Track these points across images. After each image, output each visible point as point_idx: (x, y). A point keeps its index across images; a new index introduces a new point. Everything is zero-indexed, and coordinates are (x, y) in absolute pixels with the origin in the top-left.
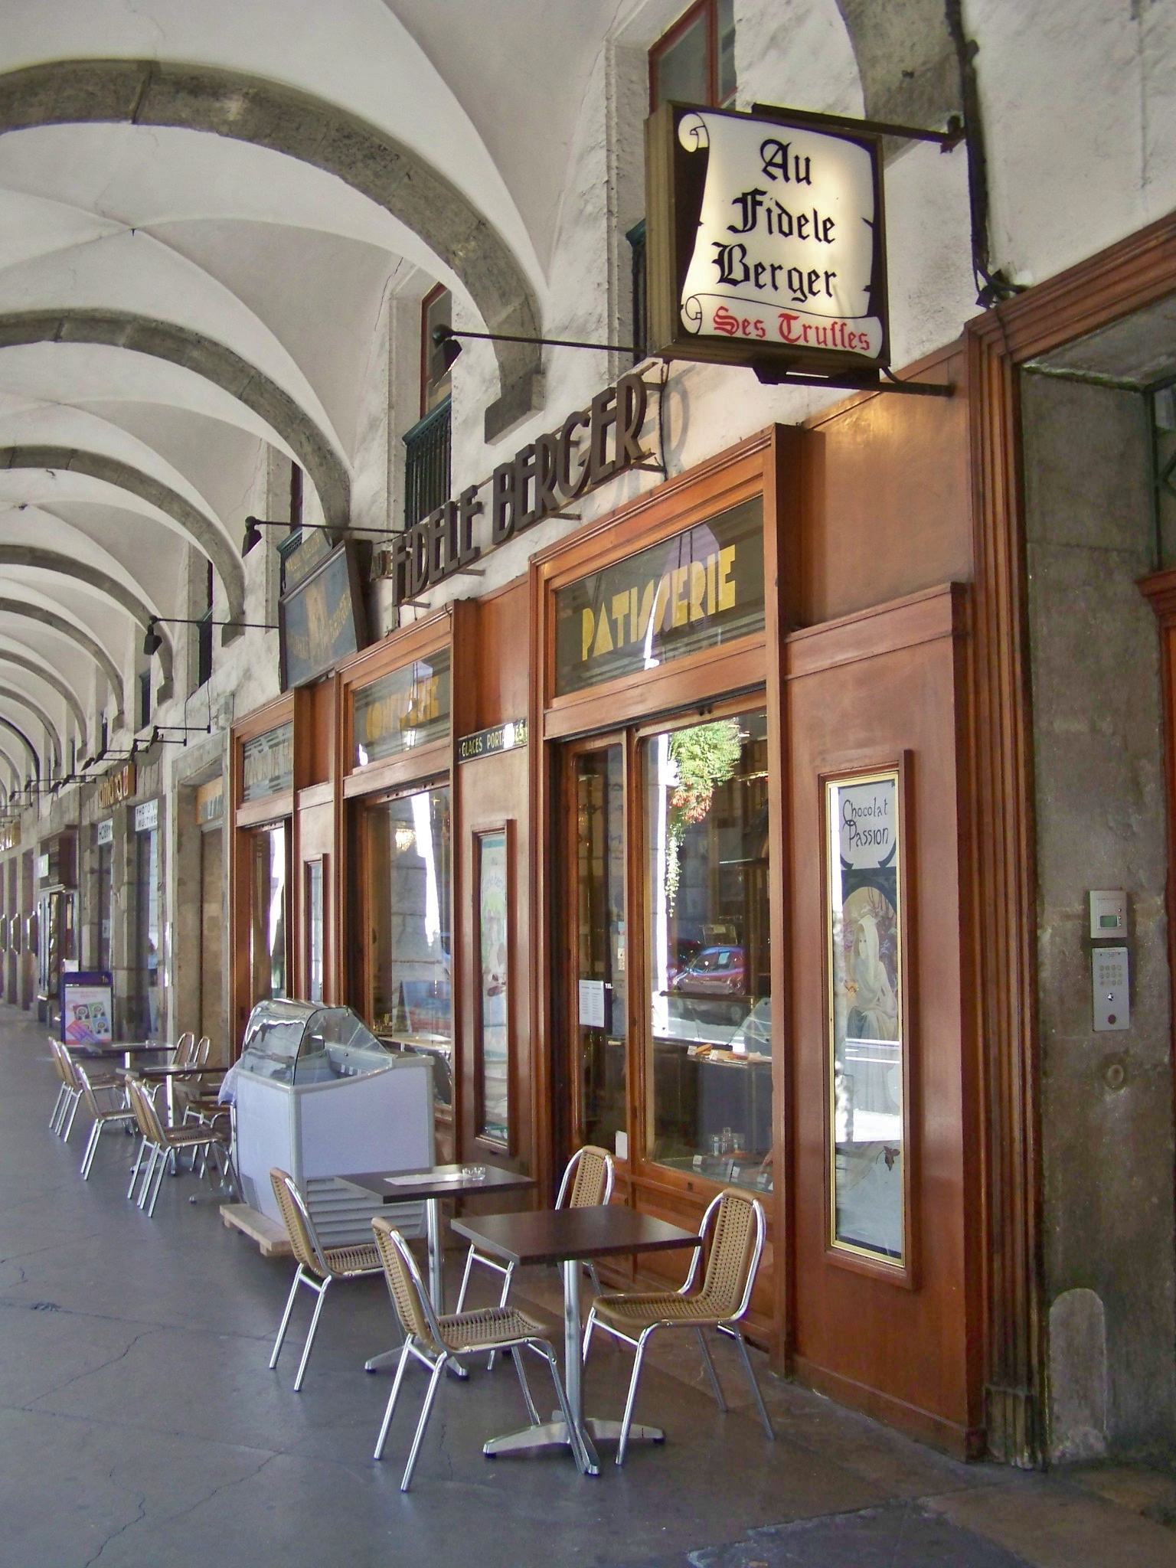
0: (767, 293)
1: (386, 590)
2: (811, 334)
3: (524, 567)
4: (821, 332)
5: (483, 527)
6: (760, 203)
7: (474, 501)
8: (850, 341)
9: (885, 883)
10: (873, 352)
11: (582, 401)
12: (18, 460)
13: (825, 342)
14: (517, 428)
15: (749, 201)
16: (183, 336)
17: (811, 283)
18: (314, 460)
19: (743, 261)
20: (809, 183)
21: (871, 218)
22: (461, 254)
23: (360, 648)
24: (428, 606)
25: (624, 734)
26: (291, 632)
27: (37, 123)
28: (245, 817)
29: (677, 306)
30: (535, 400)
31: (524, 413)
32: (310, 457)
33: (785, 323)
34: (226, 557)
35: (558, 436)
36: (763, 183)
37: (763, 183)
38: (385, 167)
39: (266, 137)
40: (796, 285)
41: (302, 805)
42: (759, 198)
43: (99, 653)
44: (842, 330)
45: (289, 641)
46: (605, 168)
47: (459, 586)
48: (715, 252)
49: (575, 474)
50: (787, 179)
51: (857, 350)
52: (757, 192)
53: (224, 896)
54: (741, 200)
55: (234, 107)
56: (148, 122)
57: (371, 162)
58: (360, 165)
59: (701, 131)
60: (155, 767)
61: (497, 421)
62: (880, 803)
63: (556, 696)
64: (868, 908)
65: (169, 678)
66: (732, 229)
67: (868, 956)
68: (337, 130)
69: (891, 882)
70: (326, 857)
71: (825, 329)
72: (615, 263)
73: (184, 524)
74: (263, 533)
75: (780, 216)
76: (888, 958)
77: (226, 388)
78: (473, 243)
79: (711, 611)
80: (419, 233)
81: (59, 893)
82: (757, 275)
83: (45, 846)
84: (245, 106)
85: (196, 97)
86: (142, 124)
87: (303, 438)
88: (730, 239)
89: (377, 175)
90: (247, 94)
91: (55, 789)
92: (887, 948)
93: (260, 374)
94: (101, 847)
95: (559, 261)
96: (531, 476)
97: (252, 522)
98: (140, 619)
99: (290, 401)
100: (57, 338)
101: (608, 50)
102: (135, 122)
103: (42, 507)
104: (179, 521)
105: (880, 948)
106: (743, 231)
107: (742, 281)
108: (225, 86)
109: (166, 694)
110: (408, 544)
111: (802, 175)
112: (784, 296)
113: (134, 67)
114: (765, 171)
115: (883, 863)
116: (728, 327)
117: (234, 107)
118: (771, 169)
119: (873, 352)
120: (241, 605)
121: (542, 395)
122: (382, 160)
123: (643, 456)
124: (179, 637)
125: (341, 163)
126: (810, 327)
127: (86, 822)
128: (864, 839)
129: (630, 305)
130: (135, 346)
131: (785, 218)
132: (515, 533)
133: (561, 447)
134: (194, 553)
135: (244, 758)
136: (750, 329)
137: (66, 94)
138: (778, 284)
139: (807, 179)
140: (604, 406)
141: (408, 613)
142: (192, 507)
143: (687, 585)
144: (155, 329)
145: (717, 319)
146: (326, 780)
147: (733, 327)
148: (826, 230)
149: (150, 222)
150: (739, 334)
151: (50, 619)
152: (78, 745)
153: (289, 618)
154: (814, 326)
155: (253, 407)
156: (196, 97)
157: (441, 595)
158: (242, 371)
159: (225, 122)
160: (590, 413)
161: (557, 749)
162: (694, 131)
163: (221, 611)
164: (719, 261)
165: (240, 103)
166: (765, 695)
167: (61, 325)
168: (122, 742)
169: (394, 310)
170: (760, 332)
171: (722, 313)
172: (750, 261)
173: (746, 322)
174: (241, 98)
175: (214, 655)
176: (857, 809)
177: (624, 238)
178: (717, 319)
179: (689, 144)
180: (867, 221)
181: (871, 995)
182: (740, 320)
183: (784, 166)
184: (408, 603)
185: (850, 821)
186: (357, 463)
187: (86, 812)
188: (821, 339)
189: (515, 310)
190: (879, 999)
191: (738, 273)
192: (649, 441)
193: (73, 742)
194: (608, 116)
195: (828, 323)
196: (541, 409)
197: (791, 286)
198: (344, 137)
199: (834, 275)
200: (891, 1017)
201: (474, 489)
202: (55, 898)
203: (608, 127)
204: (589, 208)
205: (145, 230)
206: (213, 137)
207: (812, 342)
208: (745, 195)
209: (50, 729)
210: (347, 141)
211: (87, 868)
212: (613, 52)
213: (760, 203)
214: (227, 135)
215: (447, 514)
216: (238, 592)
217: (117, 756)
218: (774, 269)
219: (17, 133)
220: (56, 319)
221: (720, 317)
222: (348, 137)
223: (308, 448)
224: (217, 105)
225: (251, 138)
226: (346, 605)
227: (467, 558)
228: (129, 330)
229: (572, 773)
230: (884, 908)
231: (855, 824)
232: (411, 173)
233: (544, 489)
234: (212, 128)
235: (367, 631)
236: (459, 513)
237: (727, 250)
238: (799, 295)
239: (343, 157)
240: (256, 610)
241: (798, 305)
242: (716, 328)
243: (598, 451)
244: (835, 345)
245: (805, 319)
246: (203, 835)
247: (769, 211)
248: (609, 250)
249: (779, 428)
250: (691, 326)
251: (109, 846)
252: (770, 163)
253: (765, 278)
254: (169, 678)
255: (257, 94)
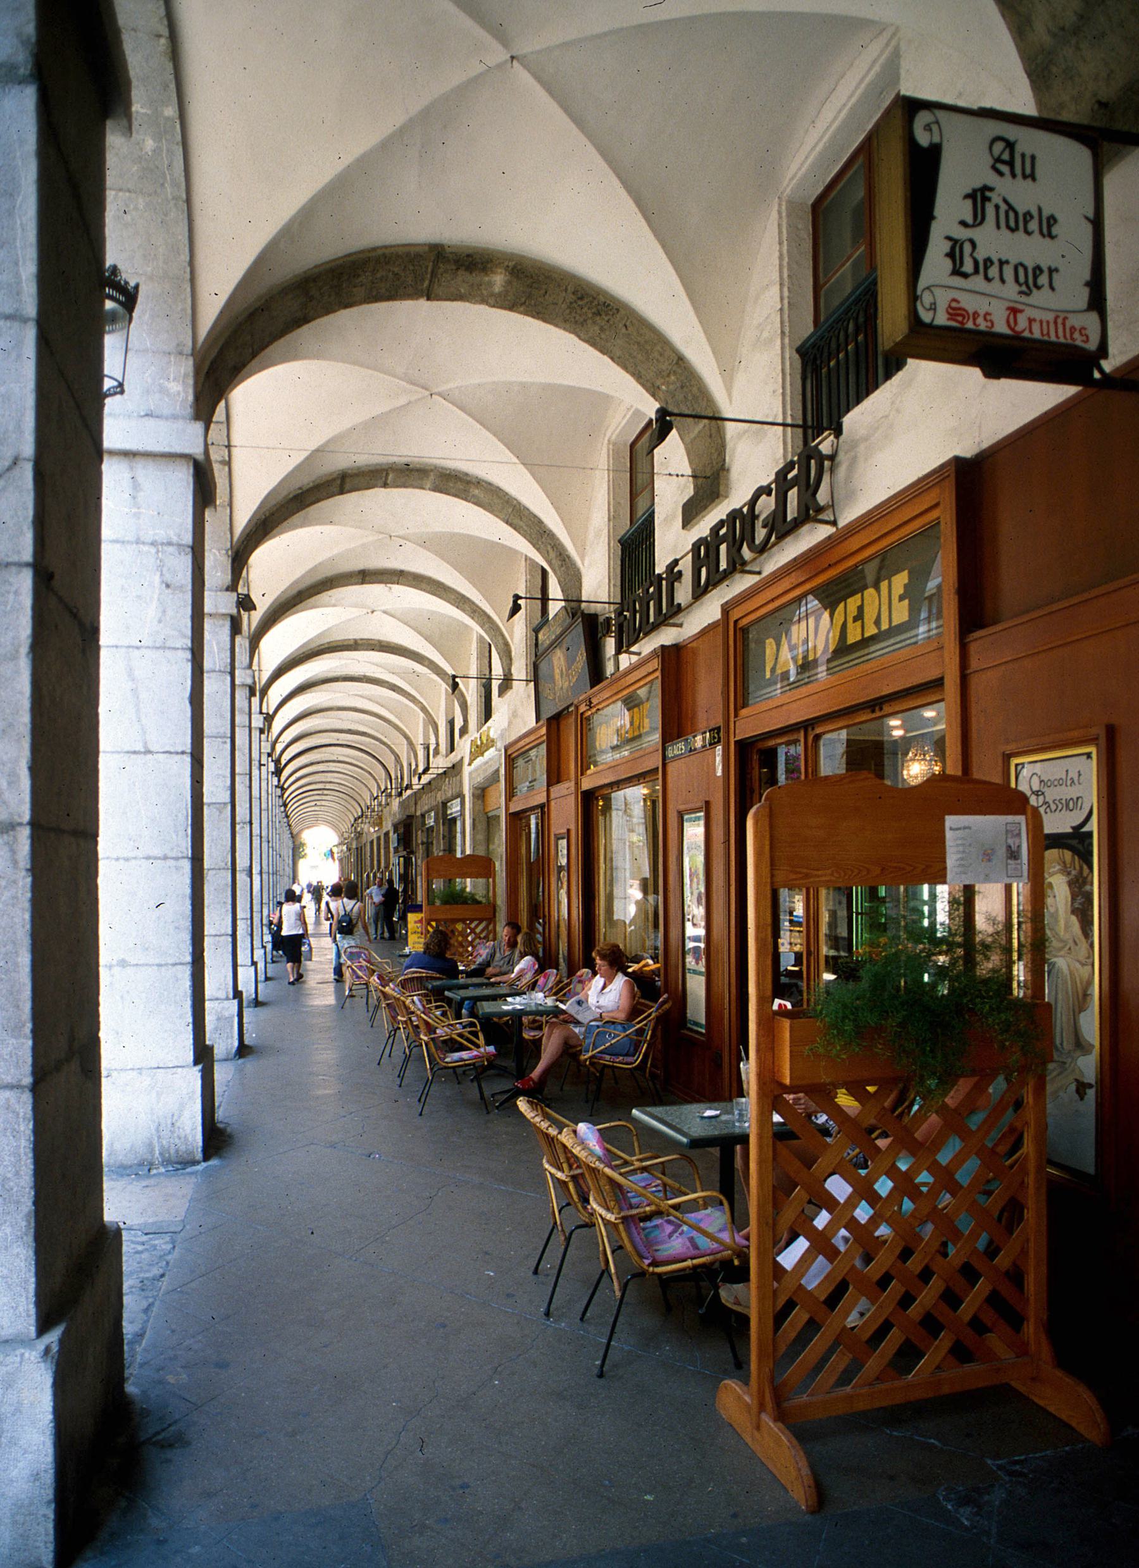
0: (995, 287)
1: (610, 644)
2: (1036, 327)
3: (717, 615)
4: (1045, 324)
5: (683, 593)
6: (989, 199)
7: (676, 570)
8: (1072, 334)
9: (1080, 847)
10: (1092, 345)
11: (767, 478)
12: (367, 578)
13: (1048, 334)
14: (708, 513)
15: (979, 197)
16: (469, 479)
17: (1035, 278)
18: (556, 563)
19: (975, 255)
20: (1034, 179)
21: (1091, 215)
22: (664, 387)
23: (592, 687)
24: (639, 654)
25: (802, 733)
26: (542, 682)
27: (361, 303)
28: (515, 807)
29: (913, 298)
30: (722, 492)
31: (713, 501)
32: (554, 561)
33: (1012, 317)
34: (500, 638)
35: (745, 510)
36: (991, 179)
37: (991, 179)
38: (608, 321)
39: (521, 305)
40: (1022, 279)
41: (552, 796)
42: (988, 194)
43: (424, 709)
44: (1064, 325)
45: (541, 688)
46: (778, 299)
47: (667, 636)
48: (946, 246)
49: (761, 534)
50: (1014, 176)
51: (1079, 343)
52: (986, 188)
53: (501, 858)
54: (972, 196)
55: (498, 280)
56: (439, 299)
57: (598, 318)
58: (589, 321)
59: (935, 128)
60: (458, 777)
61: (691, 512)
62: (1073, 774)
63: (743, 708)
64: (1058, 867)
65: (466, 720)
66: (963, 223)
67: (1057, 911)
68: (573, 293)
69: (1086, 843)
70: (568, 831)
71: (1048, 322)
72: (788, 371)
73: (473, 618)
74: (523, 606)
75: (1007, 213)
76: (1083, 914)
77: (497, 516)
78: (673, 378)
79: (885, 626)
80: (633, 375)
81: (403, 856)
82: (986, 269)
83: (396, 827)
84: (506, 278)
85: (471, 273)
86: (434, 300)
87: (549, 548)
88: (961, 233)
89: (602, 329)
90: (508, 266)
91: (400, 794)
92: (1080, 904)
93: (519, 503)
94: (428, 829)
95: (741, 379)
96: (722, 543)
97: (517, 597)
98: (447, 684)
99: (540, 522)
100: (385, 485)
101: (780, 205)
102: (428, 299)
103: (385, 612)
104: (470, 616)
105: (1072, 903)
106: (973, 226)
107: (971, 275)
108: (492, 261)
109: (464, 731)
110: (626, 608)
111: (1028, 171)
112: (1011, 290)
113: (427, 248)
114: (994, 168)
115: (1076, 828)
116: (960, 319)
117: (498, 280)
118: (999, 166)
119: (1092, 345)
120: (510, 670)
121: (727, 486)
122: (606, 315)
123: (820, 510)
124: (471, 690)
125: (576, 322)
126: (1034, 320)
127: (418, 813)
128: (1053, 807)
129: (800, 406)
130: (436, 489)
131: (1012, 215)
132: (710, 588)
133: (748, 520)
134: (481, 639)
135: (514, 768)
136: (980, 320)
137: (379, 275)
138: (1005, 277)
139: (1032, 176)
140: (786, 476)
141: (625, 661)
142: (477, 606)
143: (861, 609)
144: (449, 475)
145: (951, 311)
146: (568, 779)
147: (964, 318)
148: (1049, 227)
149: (443, 388)
150: (970, 325)
151: (394, 688)
152: (413, 767)
153: (541, 674)
154: (1038, 319)
155: (515, 529)
156: (471, 273)
157: (647, 646)
158: (507, 502)
159: (492, 295)
160: (773, 486)
161: (744, 748)
162: (928, 128)
163: (497, 670)
164: (951, 255)
165: (502, 276)
166: (943, 690)
167: (387, 474)
168: (440, 763)
169: (611, 452)
170: (989, 324)
171: (954, 305)
172: (981, 255)
173: (976, 315)
174: (504, 271)
175: (493, 704)
176: (1046, 780)
177: (794, 352)
178: (951, 311)
179: (923, 139)
180: (1087, 218)
181: (1061, 945)
182: (971, 312)
183: (1011, 164)
184: (626, 652)
185: (1038, 791)
186: (586, 563)
187: (418, 807)
188: (1045, 332)
189: (705, 426)
190: (1070, 949)
191: (968, 267)
192: (822, 497)
193: (410, 765)
194: (781, 258)
195: (1050, 317)
196: (727, 497)
197: (1017, 280)
198: (579, 299)
199: (1057, 270)
200: (1083, 965)
201: (676, 562)
202: (402, 859)
203: (781, 266)
204: (765, 334)
205: (439, 394)
206: (483, 308)
207: (1037, 334)
208: (975, 191)
209: (397, 758)
210: (580, 303)
211: (420, 842)
212: (784, 207)
213: (989, 199)
214: (494, 306)
215: (656, 584)
216: (508, 662)
217: (436, 771)
218: (1002, 263)
219: (347, 311)
220: (384, 470)
221: (954, 309)
222: (581, 298)
223: (552, 555)
224: (487, 279)
225: (511, 308)
226: (581, 657)
227: (672, 614)
228: (432, 477)
229: (756, 765)
230: (1077, 867)
231: (1043, 793)
232: (628, 324)
233: (734, 550)
234: (484, 301)
235: (596, 673)
236: (664, 582)
237: (958, 245)
238: (1024, 288)
239: (578, 317)
240: (520, 670)
241: (1024, 299)
242: (948, 319)
243: (781, 508)
244: (1057, 336)
245: (1030, 312)
246: (488, 818)
247: (997, 207)
248: (783, 363)
249: (957, 461)
250: (926, 317)
251: (432, 827)
252: (998, 160)
253: (993, 272)
254: (466, 720)
255: (515, 267)
